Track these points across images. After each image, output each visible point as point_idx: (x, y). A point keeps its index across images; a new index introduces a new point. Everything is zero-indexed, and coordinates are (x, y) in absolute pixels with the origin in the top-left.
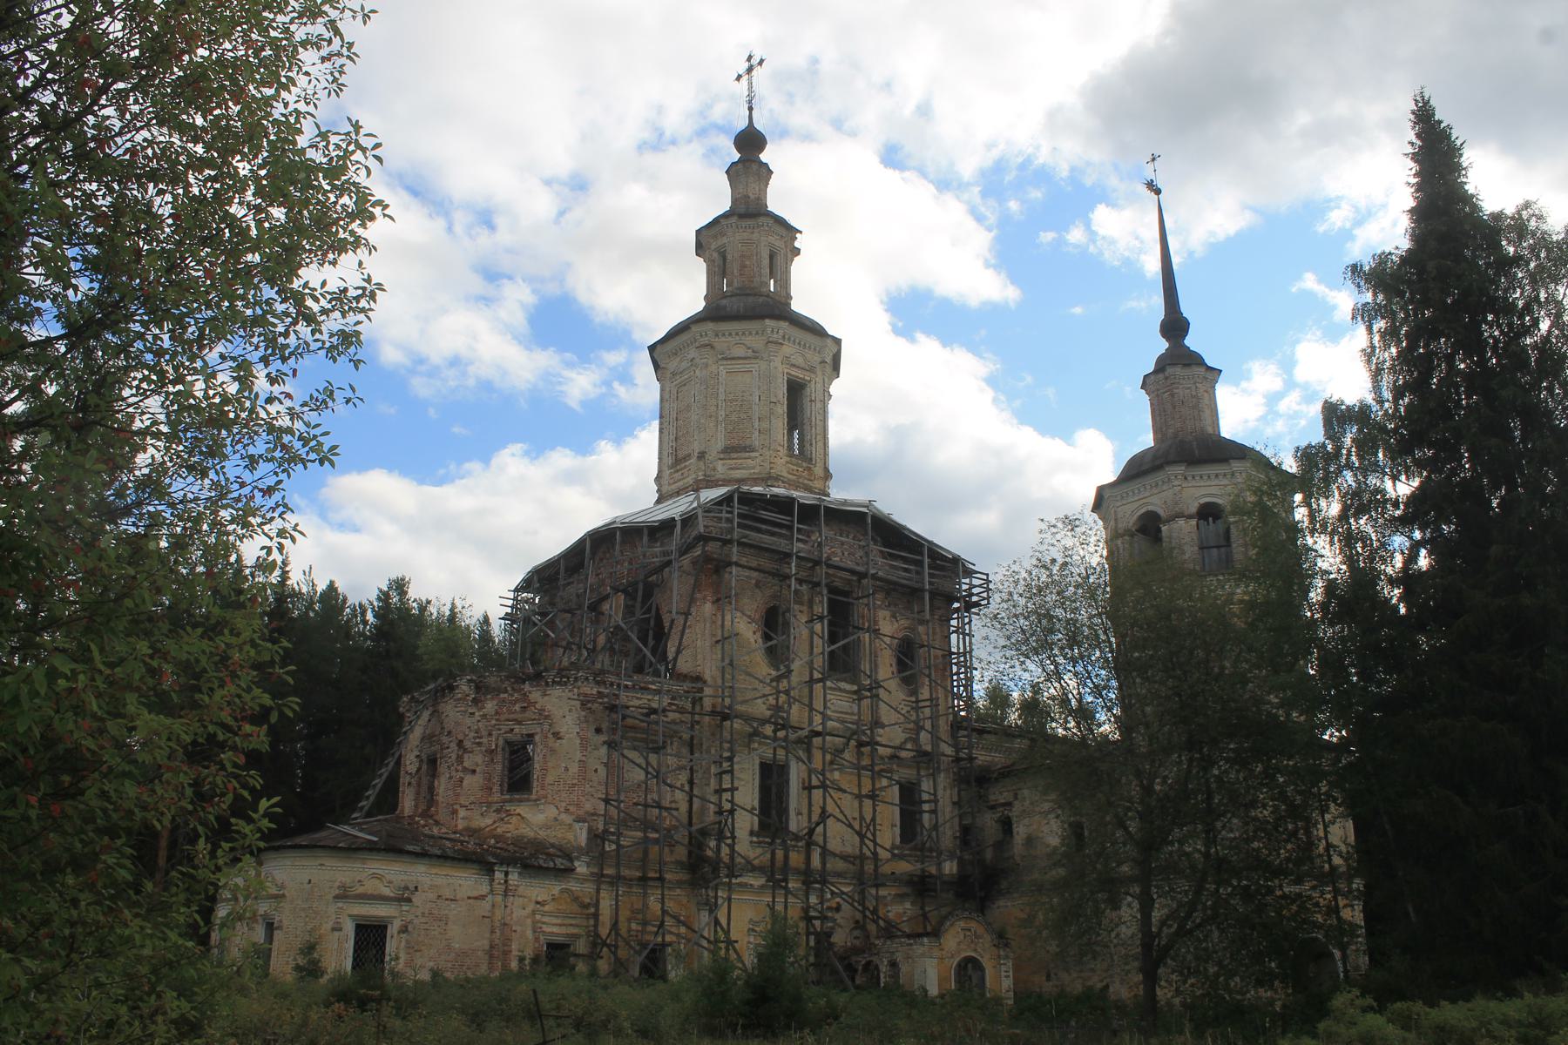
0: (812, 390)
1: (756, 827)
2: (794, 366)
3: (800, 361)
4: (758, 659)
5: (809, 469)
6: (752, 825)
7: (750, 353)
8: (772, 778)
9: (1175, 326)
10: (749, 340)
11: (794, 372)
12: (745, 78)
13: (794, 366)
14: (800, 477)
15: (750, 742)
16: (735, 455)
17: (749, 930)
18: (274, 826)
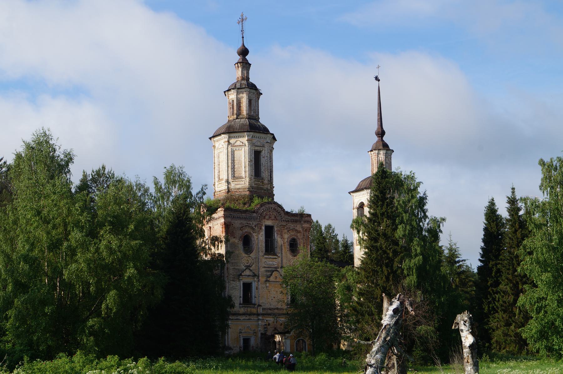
0: (264, 153)
1: (242, 302)
2: (256, 146)
3: (259, 144)
4: (241, 252)
5: (262, 182)
6: (240, 302)
7: (241, 144)
8: (247, 287)
9: (381, 133)
10: (241, 139)
11: (257, 148)
12: (241, 23)
13: (256, 146)
14: (259, 185)
15: (239, 277)
16: (237, 180)
17: (240, 332)
18: (133, 357)
